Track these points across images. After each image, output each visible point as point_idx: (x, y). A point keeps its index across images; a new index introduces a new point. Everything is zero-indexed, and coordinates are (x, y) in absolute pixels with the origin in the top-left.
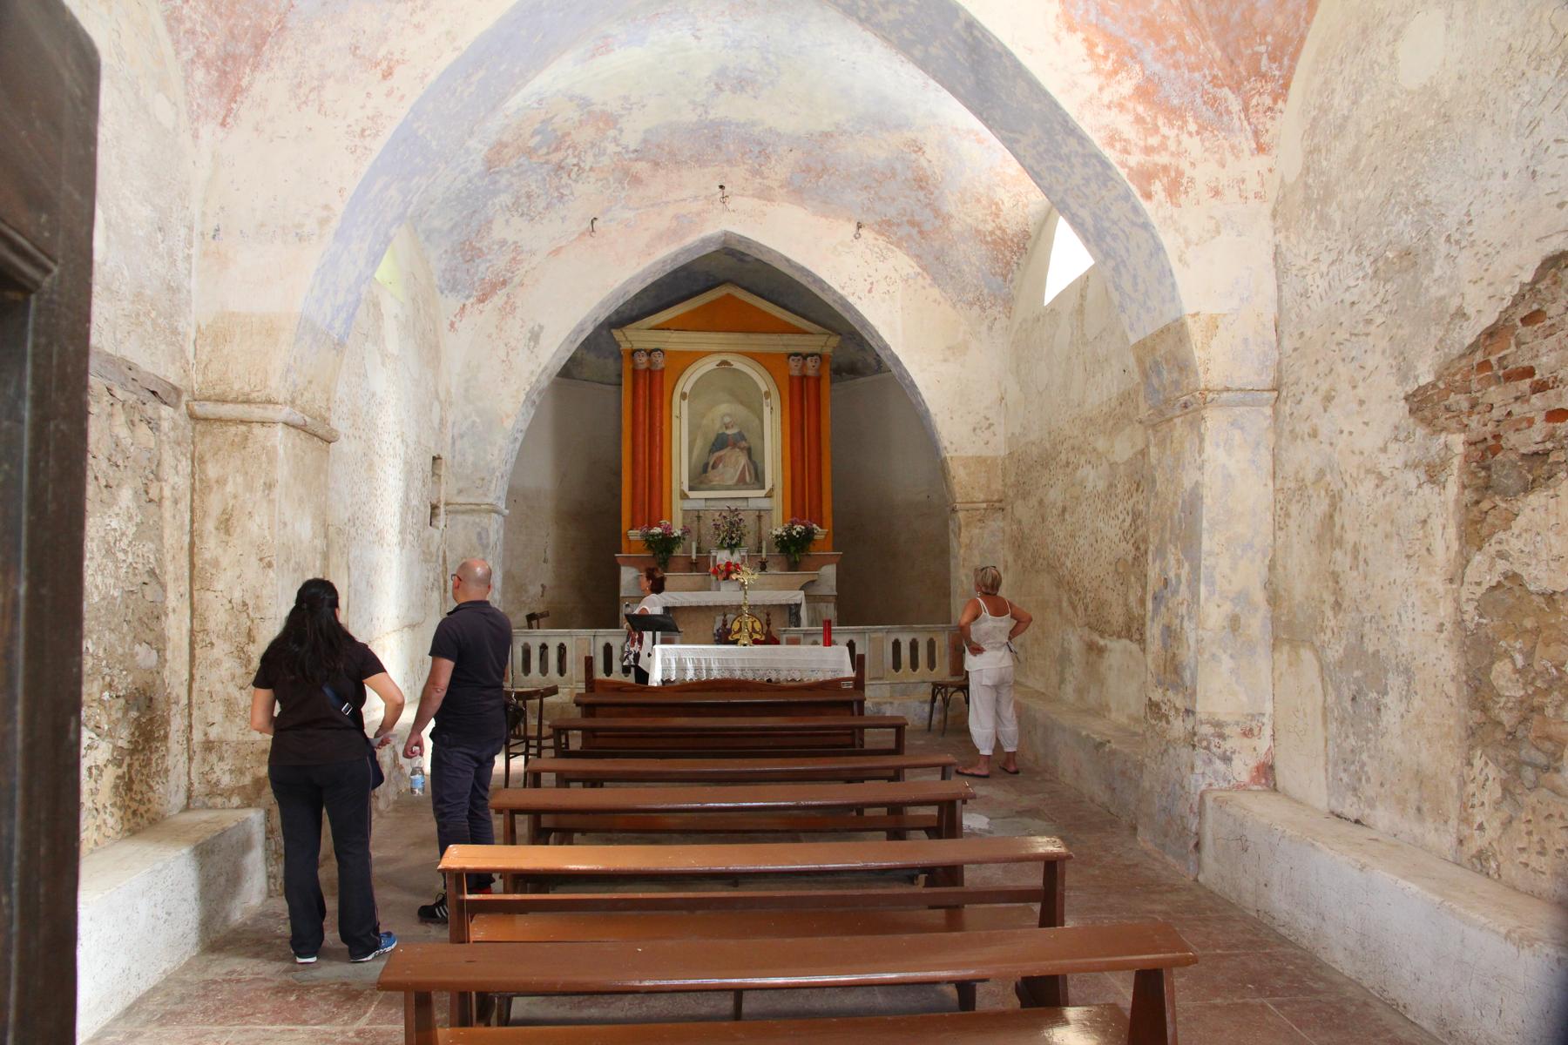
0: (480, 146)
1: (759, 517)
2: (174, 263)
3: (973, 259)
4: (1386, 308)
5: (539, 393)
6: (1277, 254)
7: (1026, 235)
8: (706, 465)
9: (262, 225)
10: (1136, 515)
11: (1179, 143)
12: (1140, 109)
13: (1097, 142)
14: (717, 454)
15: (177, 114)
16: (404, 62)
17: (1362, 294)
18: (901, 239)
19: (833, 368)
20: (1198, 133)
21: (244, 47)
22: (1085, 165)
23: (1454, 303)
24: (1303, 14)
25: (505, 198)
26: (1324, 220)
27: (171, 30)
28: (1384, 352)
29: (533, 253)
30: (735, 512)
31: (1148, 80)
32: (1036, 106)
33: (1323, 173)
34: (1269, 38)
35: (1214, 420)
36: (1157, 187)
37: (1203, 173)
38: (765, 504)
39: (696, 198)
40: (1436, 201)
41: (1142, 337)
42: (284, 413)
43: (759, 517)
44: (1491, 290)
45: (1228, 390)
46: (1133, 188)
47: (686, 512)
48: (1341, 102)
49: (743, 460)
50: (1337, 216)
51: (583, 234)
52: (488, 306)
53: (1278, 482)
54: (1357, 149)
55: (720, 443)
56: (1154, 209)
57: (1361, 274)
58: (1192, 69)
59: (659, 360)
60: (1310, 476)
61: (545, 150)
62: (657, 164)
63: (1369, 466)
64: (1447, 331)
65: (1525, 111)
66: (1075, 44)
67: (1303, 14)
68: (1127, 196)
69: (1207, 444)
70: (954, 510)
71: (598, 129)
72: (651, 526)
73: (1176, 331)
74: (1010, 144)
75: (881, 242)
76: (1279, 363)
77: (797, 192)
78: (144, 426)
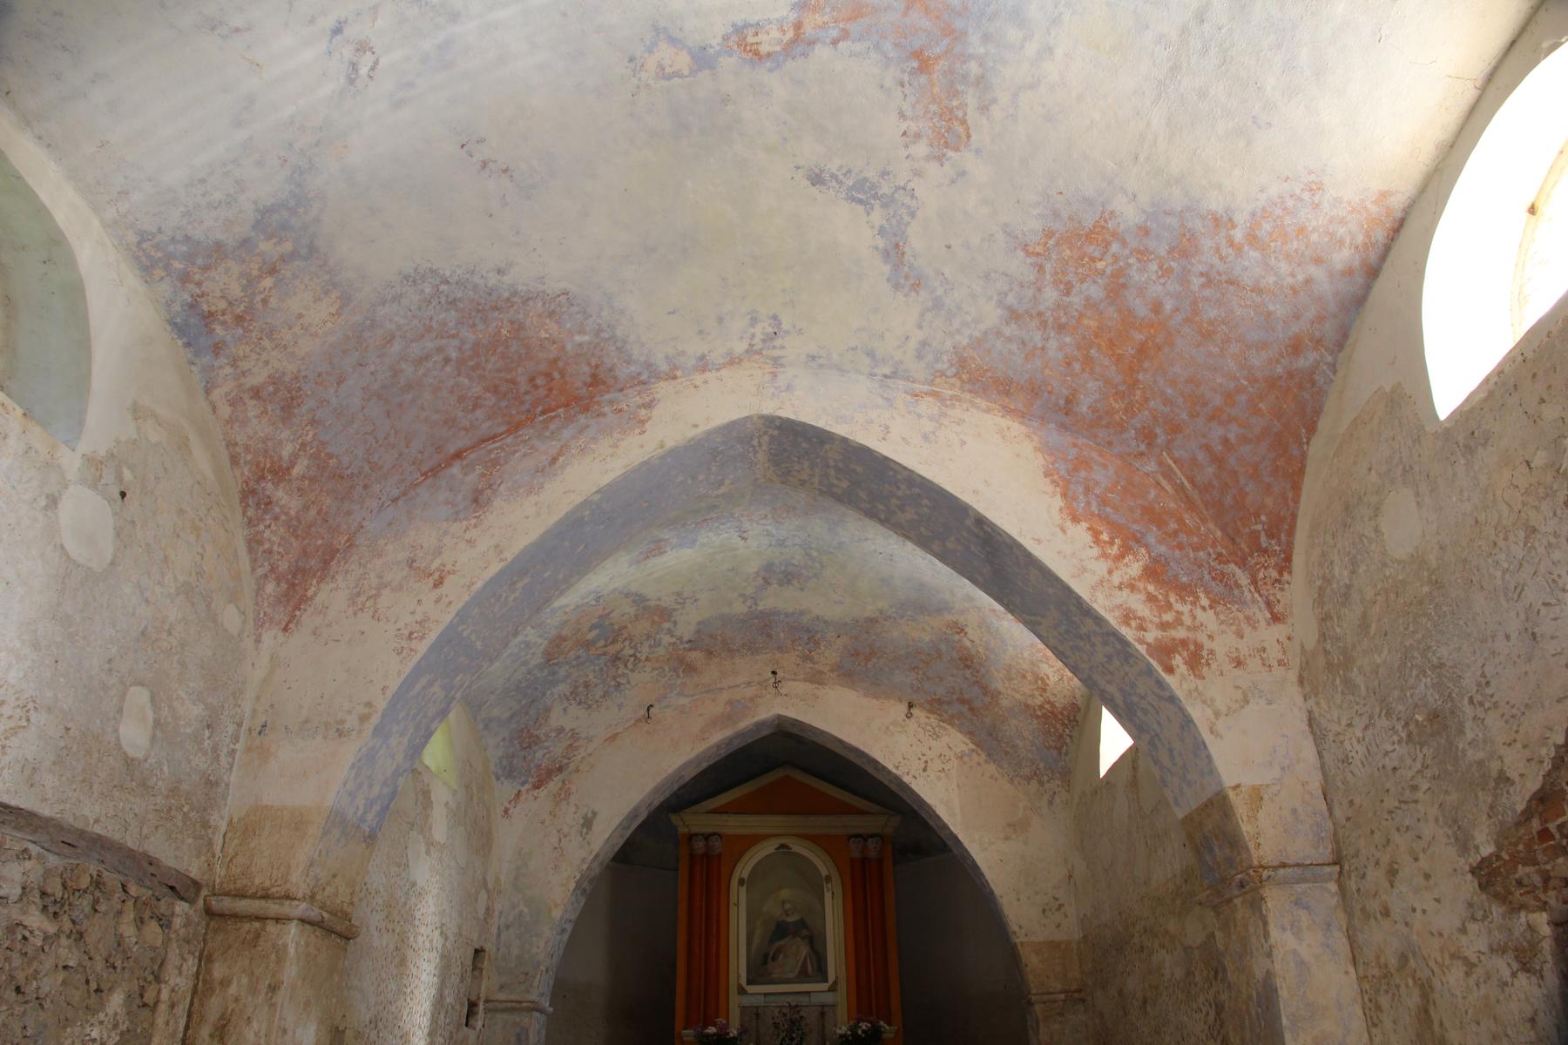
0: (540, 641)
1: (823, 1014)
2: (217, 758)
3: (1026, 734)
4: (1428, 773)
5: (591, 881)
6: (1311, 721)
7: (1074, 707)
8: (766, 956)
9: (307, 721)
10: (1220, 1008)
11: (1194, 617)
12: (1151, 588)
13: (1113, 622)
14: (777, 944)
15: (244, 622)
16: (454, 572)
17: (1401, 759)
18: (952, 716)
19: (893, 846)
20: (1211, 607)
21: (313, 563)
22: (1105, 643)
23: (1495, 766)
24: (1290, 495)
25: (563, 688)
26: (1349, 685)
27: (251, 550)
28: (1437, 820)
29: (590, 740)
30: (795, 1008)
31: (1155, 560)
32: (1050, 591)
33: (1338, 639)
34: (1263, 518)
35: (1275, 900)
36: (1178, 661)
37: (1222, 645)
38: (828, 998)
39: (749, 684)
40: (1449, 664)
41: (1187, 811)
42: (301, 909)
43: (823, 1014)
44: (1527, 753)
45: (1284, 865)
46: (1154, 663)
47: (743, 1009)
48: (1341, 573)
49: (804, 951)
50: (1360, 681)
51: (639, 720)
52: (543, 793)
53: (1361, 970)
54: (1364, 615)
55: (781, 931)
56: (1178, 682)
57: (1395, 738)
58: (1196, 549)
59: (717, 844)
60: (1393, 962)
61: (602, 643)
62: (710, 653)
63: (1452, 950)
64: (1495, 796)
65: (1507, 577)
66: (1080, 533)
67: (1290, 495)
68: (1150, 671)
69: (1271, 927)
70: (1030, 1003)
71: (653, 622)
72: (706, 1026)
73: (1219, 805)
74: (1033, 626)
75: (933, 720)
76: (1335, 834)
77: (847, 676)
78: (154, 925)
